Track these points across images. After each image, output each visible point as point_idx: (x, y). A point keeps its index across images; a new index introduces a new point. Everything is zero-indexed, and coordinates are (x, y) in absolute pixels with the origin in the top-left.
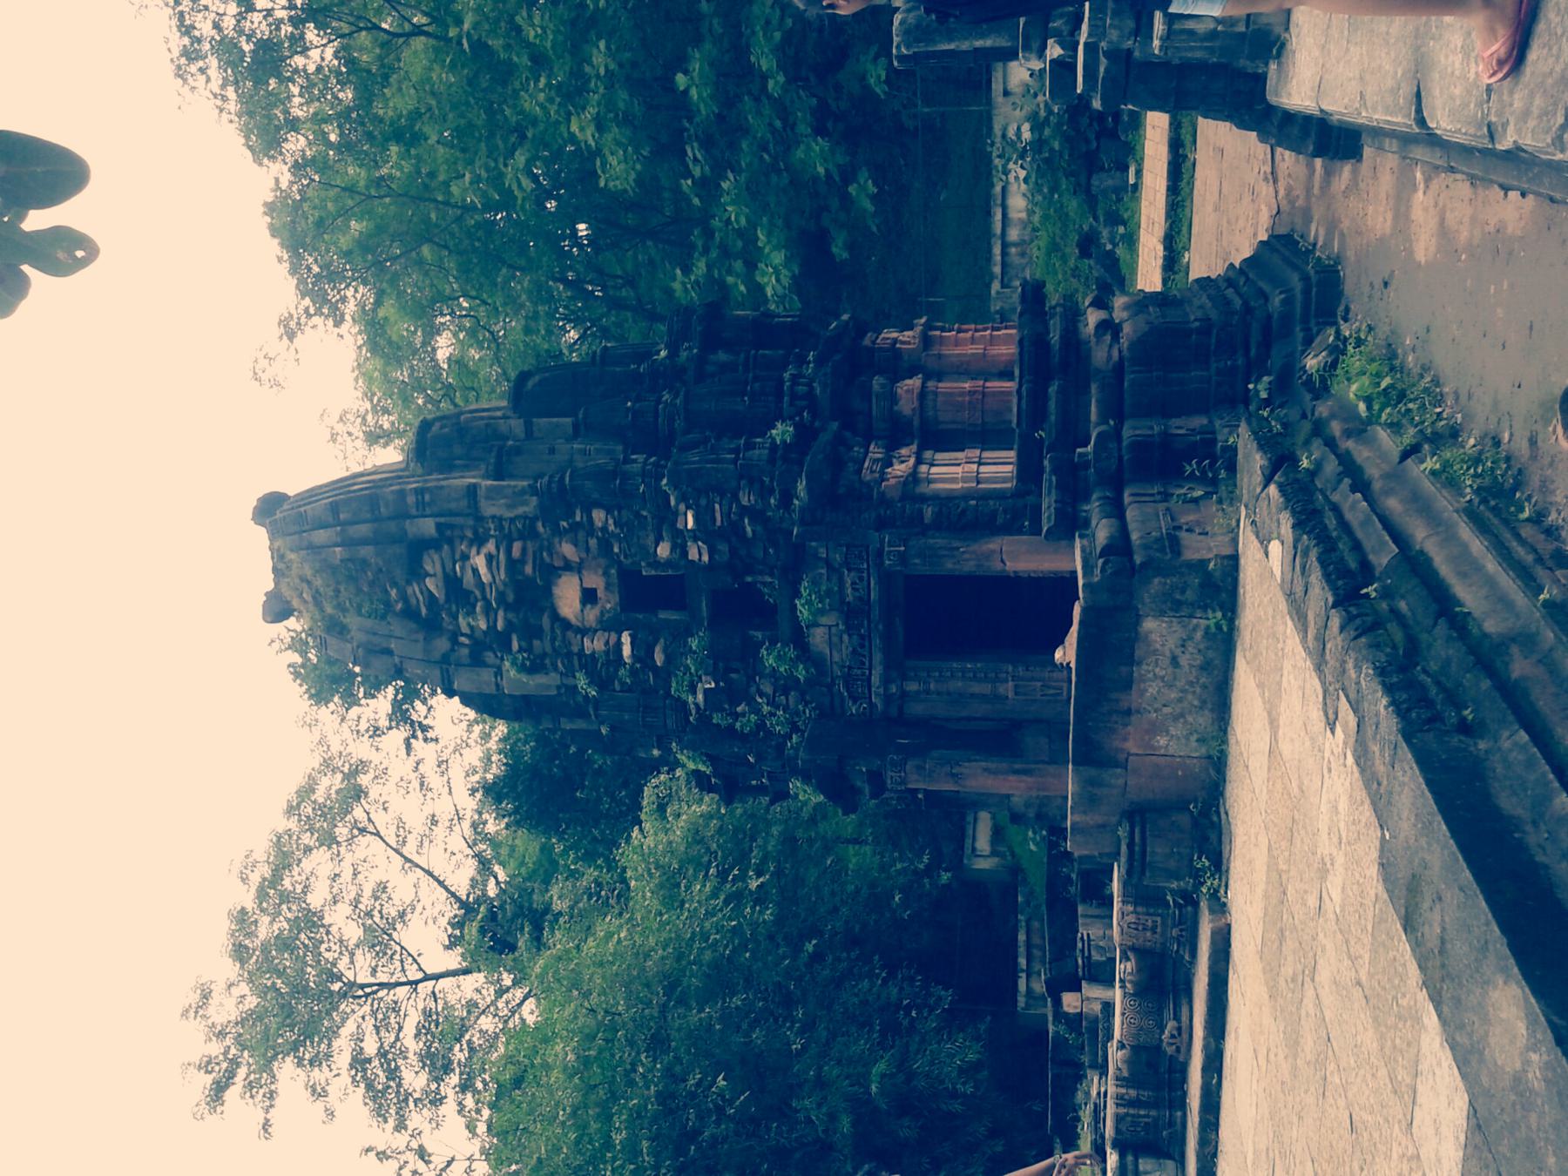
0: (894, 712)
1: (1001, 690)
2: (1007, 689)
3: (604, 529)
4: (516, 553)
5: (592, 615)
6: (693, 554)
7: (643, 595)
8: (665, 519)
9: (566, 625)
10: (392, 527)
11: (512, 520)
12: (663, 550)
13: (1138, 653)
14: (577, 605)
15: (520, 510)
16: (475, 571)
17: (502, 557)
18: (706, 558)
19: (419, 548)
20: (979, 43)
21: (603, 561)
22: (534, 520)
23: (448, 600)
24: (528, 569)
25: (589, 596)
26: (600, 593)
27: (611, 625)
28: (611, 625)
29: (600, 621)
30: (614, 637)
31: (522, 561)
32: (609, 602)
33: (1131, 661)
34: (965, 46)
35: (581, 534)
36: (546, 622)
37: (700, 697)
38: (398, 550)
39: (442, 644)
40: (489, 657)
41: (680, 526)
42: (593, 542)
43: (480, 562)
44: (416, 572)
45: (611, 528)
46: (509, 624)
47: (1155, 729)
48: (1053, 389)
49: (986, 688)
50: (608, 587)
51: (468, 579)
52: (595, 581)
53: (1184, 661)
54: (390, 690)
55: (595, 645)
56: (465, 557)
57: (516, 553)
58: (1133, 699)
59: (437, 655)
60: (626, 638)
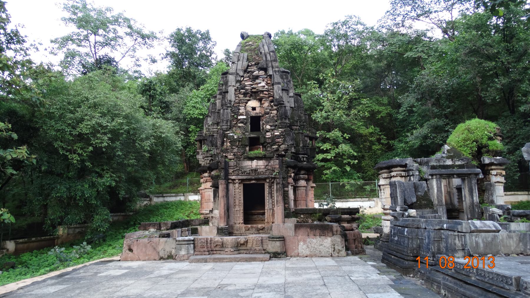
0: (230, 181)
1: (237, 207)
2: (237, 208)
3: (271, 113)
4: (265, 92)
5: (250, 109)
6: (268, 134)
7: (255, 122)
8: (276, 127)
9: (247, 103)
10: (270, 65)
11: (273, 92)
12: (268, 127)
13: (322, 237)
14: (252, 106)
15: (275, 94)
16: (260, 83)
17: (264, 89)
18: (267, 137)
19: (265, 70)
20: (399, 198)
21: (263, 113)
22: (273, 97)
23: (253, 76)
24: (261, 95)
25: (254, 109)
26: (255, 111)
27: (247, 114)
28: (247, 114)
29: (248, 111)
30: (245, 114)
31: (263, 94)
32: (253, 113)
33: (320, 236)
34: (398, 195)
35: (270, 108)
36: (248, 98)
37: (231, 134)
38: (265, 66)
39: (241, 74)
40: (238, 84)
41: (276, 131)
42: (268, 110)
43: (263, 84)
44: (261, 69)
45: (272, 115)
46: (247, 90)
47: (304, 241)
48: (348, 216)
49: (237, 203)
50: (256, 113)
51: (258, 81)
52: (258, 110)
53: (321, 247)
54: (177, 52)
55: (242, 110)
56: (263, 80)
57: (265, 92)
58: (311, 235)
59: (238, 72)
60: (245, 117)
